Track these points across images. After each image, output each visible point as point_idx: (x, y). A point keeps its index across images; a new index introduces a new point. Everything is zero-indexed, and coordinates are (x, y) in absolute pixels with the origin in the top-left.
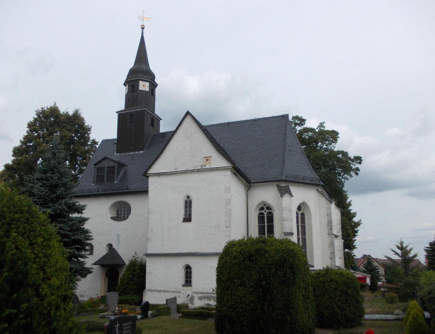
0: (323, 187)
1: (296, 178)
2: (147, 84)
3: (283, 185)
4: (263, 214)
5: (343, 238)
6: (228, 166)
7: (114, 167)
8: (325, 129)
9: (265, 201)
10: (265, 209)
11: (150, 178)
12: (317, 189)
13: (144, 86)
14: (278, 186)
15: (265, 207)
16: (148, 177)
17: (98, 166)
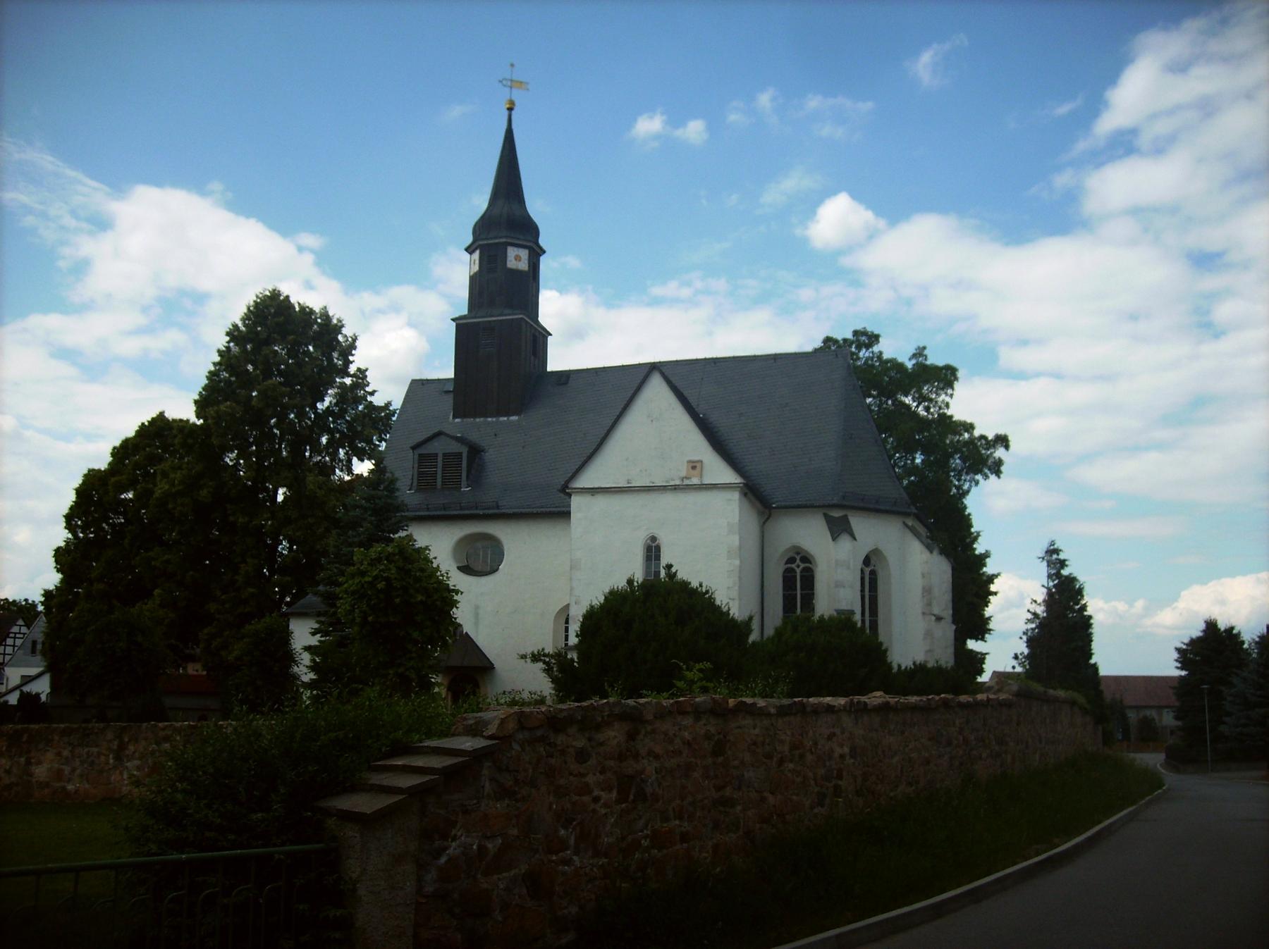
0: (918, 517)
1: (862, 500)
2: (524, 254)
3: (836, 514)
4: (793, 570)
5: (954, 622)
6: (736, 482)
7: (460, 454)
8: (928, 362)
9: (798, 545)
10: (798, 561)
11: (572, 497)
12: (904, 523)
13: (517, 259)
14: (826, 515)
15: (798, 558)
16: (570, 495)
17: (423, 451)
